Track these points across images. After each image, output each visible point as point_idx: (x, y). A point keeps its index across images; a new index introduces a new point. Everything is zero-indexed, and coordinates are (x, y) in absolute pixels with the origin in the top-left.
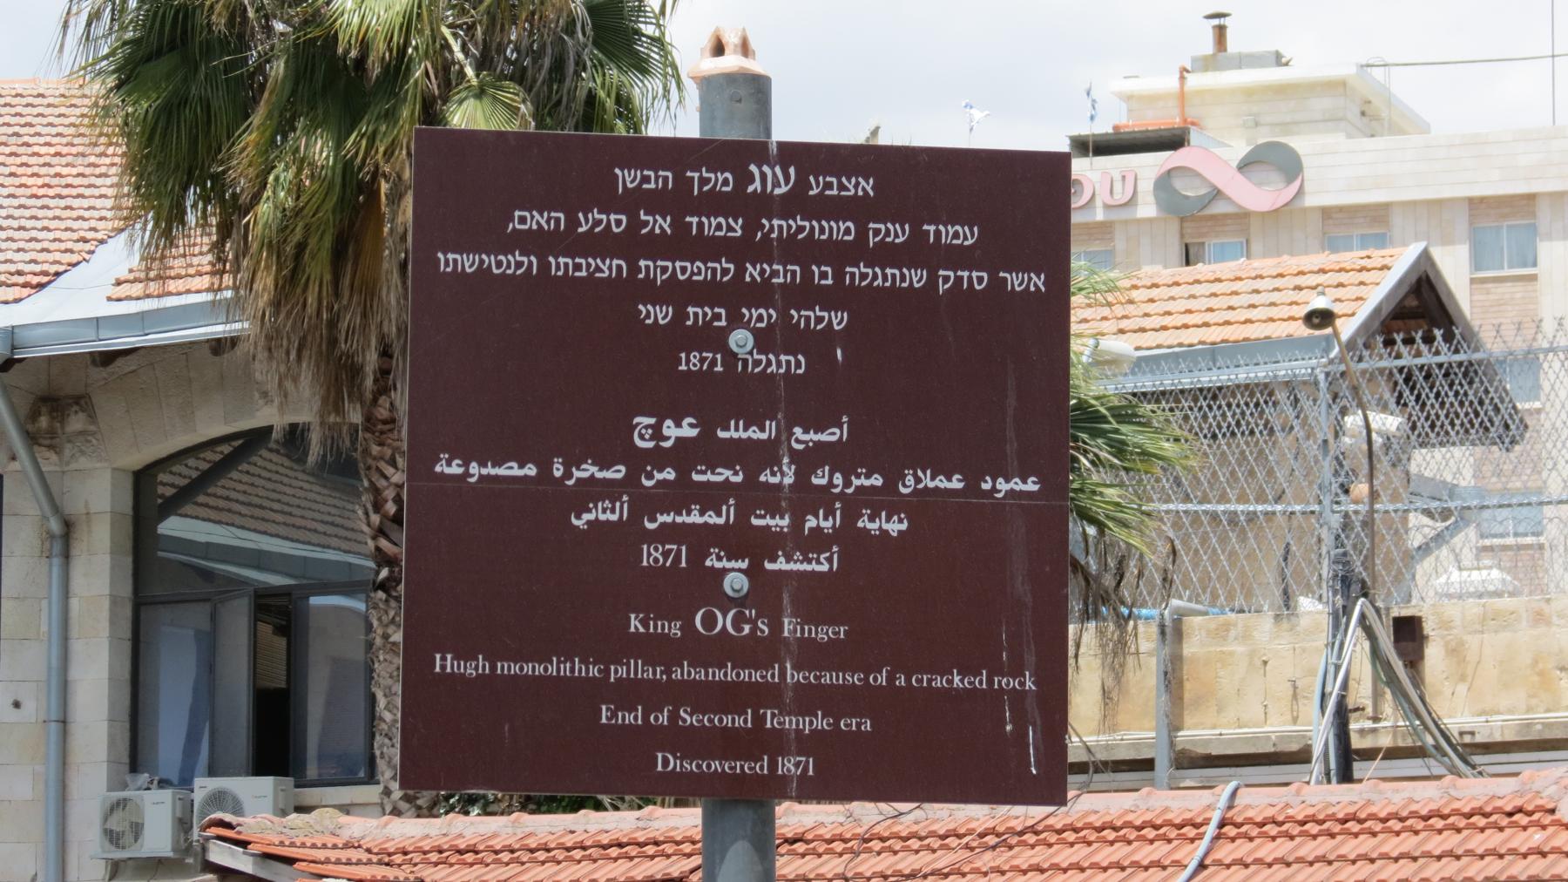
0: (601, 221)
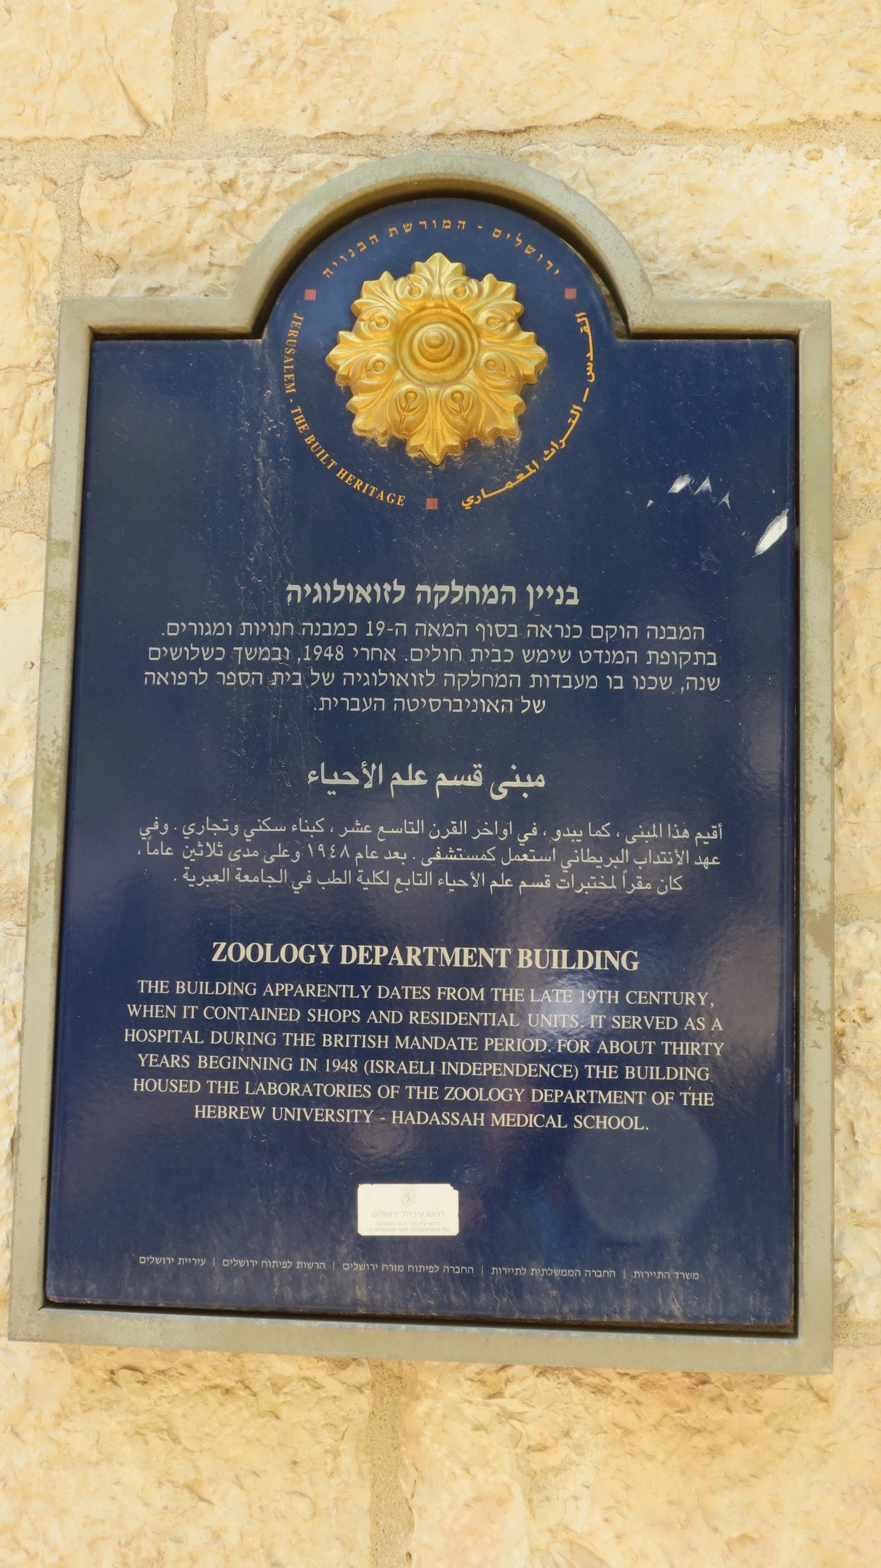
0: (457, 593)
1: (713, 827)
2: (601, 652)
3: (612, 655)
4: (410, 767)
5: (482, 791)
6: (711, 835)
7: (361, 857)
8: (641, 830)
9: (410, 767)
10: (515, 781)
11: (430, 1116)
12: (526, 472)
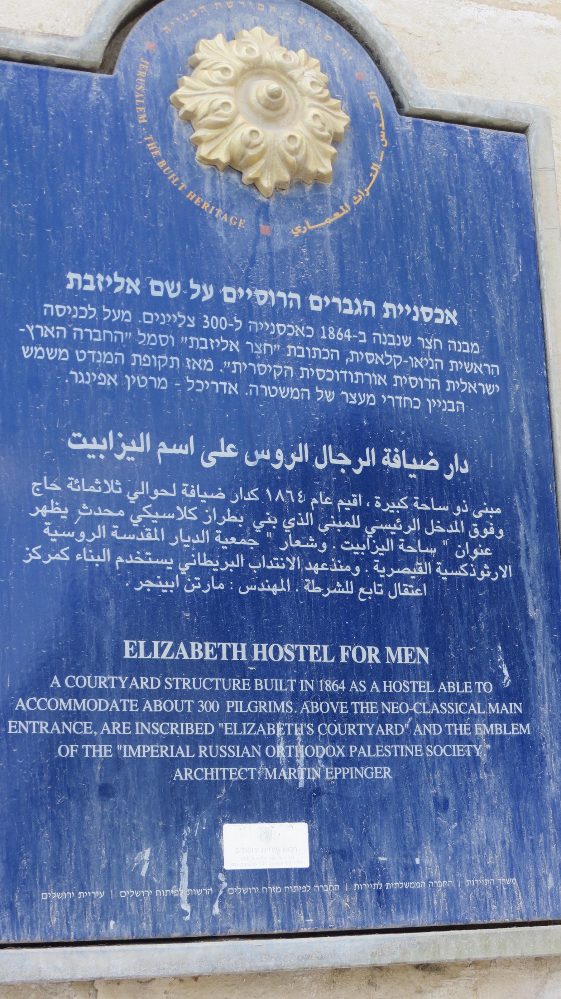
1: (353, 496)
2: (93, 352)
3: (103, 356)
4: (222, 441)
5: (194, 459)
6: (352, 502)
7: (317, 502)
8: (486, 506)
9: (222, 441)
10: (82, 443)
11: (110, 703)
12: (341, 211)
